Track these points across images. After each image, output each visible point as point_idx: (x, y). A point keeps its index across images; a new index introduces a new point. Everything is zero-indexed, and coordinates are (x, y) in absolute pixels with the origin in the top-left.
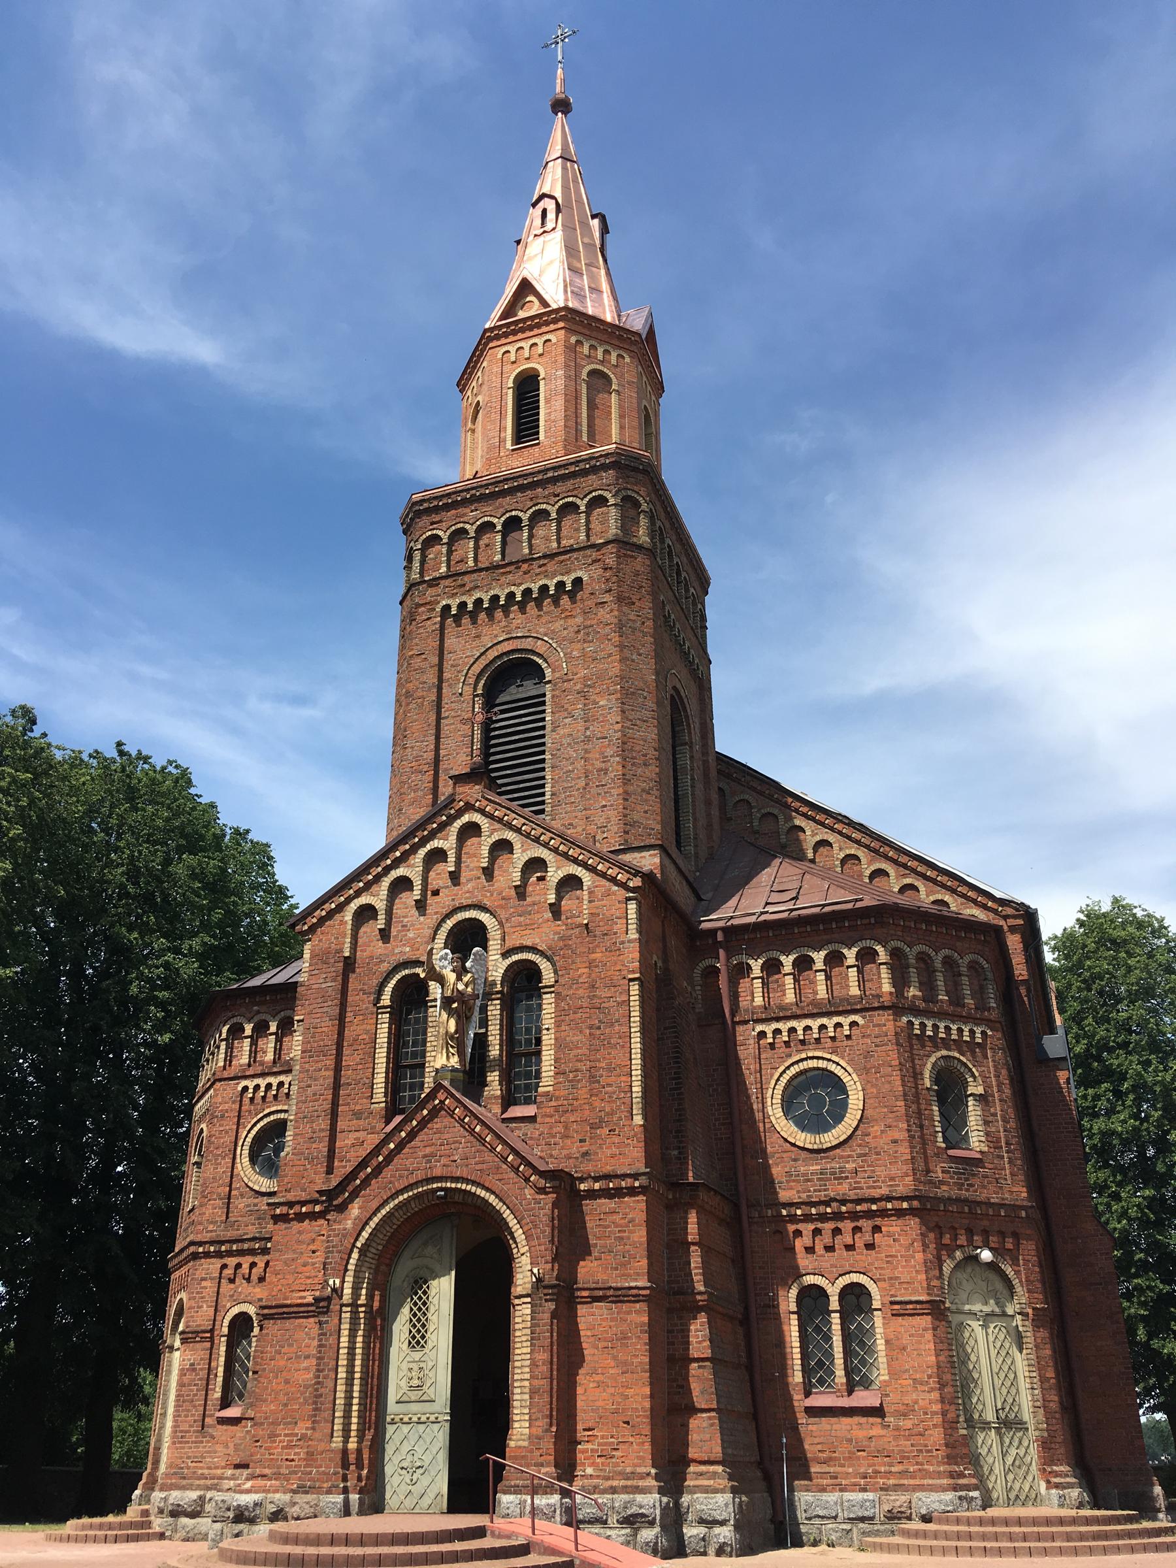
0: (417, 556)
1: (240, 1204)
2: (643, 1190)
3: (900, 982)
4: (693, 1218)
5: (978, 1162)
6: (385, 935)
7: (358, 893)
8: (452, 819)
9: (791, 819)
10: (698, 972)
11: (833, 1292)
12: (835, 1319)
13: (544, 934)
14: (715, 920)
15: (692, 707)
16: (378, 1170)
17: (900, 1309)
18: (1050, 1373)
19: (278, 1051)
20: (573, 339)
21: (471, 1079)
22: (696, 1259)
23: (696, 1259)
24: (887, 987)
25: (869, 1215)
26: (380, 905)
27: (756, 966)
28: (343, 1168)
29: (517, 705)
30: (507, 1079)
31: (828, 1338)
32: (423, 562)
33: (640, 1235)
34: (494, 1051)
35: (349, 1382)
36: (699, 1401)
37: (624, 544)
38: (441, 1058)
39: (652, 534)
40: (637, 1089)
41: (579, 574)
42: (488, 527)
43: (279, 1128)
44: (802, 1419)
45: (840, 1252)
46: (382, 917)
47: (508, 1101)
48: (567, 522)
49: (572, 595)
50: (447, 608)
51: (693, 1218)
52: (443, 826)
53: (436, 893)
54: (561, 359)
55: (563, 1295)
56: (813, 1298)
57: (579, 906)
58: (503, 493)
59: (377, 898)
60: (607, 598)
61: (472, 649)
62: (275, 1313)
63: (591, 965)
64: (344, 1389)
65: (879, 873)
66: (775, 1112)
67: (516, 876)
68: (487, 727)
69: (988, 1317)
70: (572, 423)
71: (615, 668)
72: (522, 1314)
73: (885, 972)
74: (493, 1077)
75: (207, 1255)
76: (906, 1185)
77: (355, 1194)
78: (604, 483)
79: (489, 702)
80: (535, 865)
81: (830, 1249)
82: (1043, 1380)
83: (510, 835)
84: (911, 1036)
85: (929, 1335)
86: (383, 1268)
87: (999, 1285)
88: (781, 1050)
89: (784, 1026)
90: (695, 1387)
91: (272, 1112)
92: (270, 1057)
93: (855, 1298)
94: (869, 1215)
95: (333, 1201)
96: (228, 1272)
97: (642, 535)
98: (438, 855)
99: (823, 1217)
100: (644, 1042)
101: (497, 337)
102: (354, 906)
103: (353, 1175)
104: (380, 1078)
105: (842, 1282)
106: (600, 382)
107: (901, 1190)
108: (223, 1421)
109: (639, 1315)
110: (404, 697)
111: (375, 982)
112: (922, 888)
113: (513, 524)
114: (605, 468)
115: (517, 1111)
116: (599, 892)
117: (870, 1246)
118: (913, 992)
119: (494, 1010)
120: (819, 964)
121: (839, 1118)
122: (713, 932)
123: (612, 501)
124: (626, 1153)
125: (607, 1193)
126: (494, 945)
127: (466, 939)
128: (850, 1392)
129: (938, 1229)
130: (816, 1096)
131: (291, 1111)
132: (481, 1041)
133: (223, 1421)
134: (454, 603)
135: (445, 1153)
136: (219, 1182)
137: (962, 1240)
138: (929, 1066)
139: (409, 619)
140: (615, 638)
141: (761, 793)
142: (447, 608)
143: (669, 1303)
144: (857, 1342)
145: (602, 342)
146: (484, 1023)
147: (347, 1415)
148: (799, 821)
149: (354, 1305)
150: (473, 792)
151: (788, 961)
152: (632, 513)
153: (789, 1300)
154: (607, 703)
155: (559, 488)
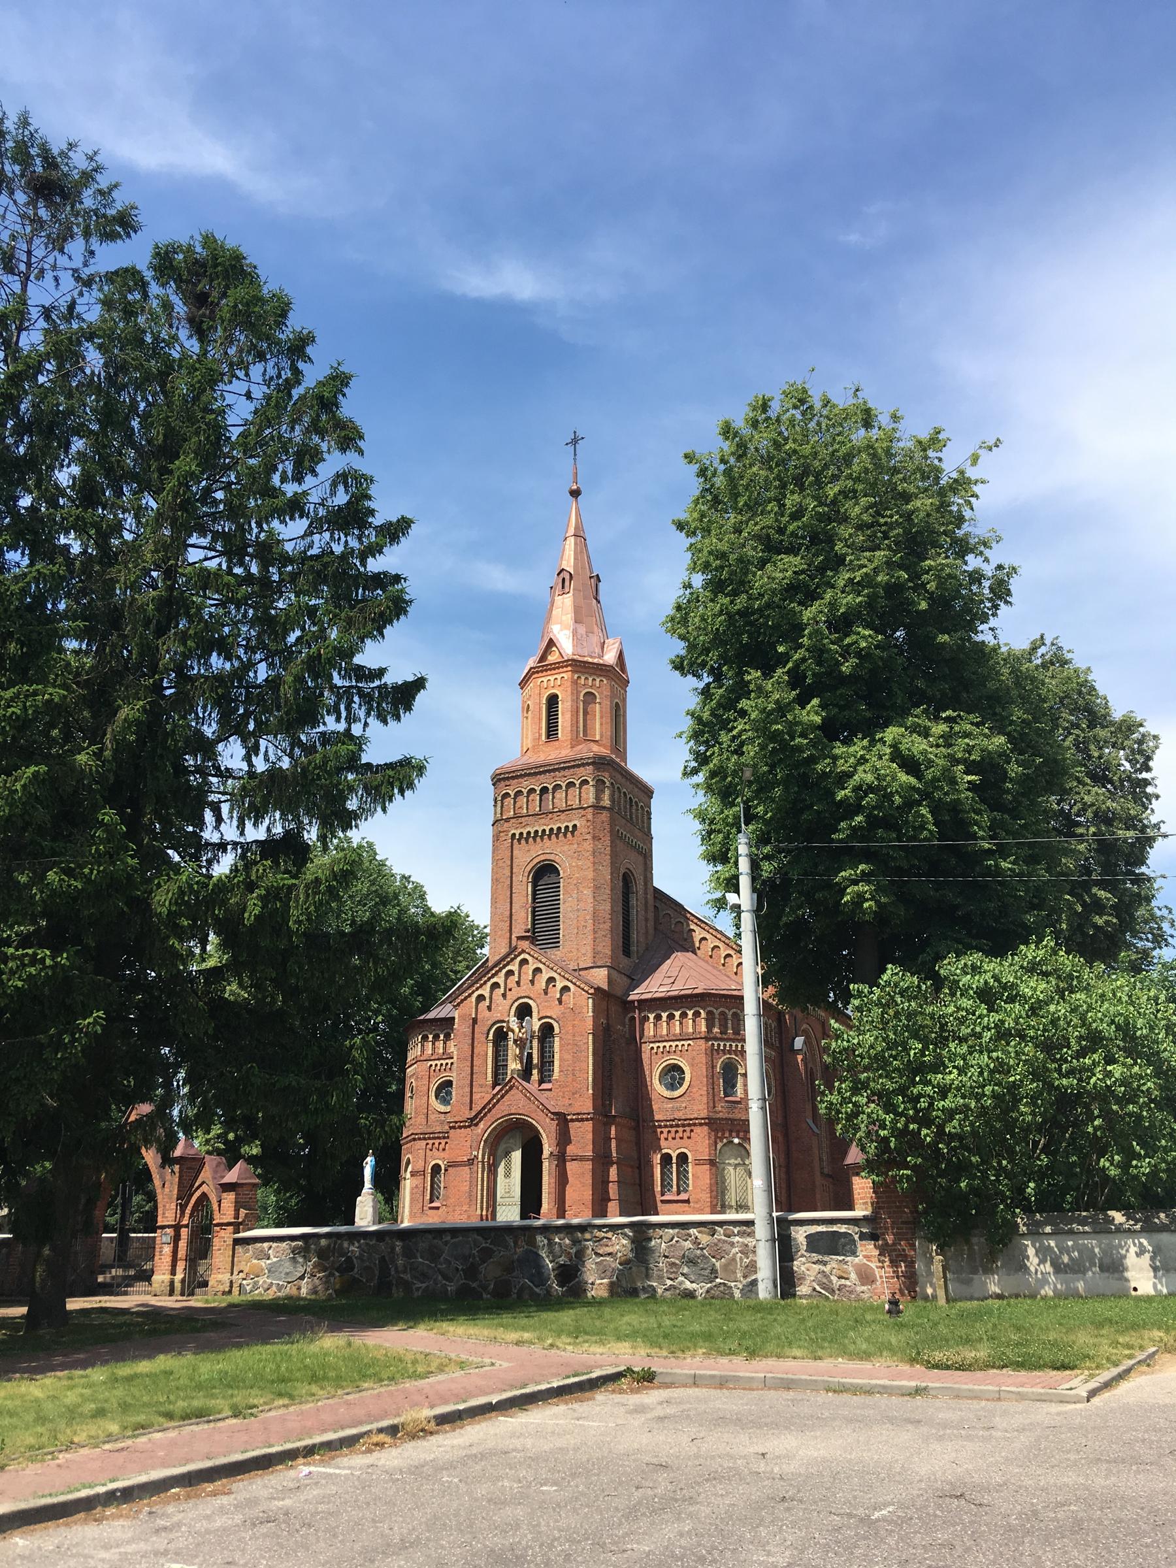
0: (499, 803)
1: (432, 1117)
2: (592, 1119)
3: (710, 1027)
4: (613, 1128)
6: (489, 1008)
7: (477, 989)
8: (516, 956)
9: (688, 925)
10: (627, 1020)
11: (674, 1156)
12: (674, 1166)
13: (555, 1011)
14: (634, 996)
16: (490, 1110)
17: (698, 1163)
19: (445, 1048)
20: (576, 676)
21: (526, 1074)
22: (613, 1144)
23: (613, 1144)
24: (704, 1029)
25: (689, 1125)
26: (487, 995)
27: (651, 1016)
28: (477, 1108)
30: (541, 1072)
32: (502, 807)
33: (590, 1136)
34: (535, 1061)
35: (482, 1190)
36: (612, 1196)
37: (597, 807)
38: (514, 1066)
39: (612, 799)
40: (590, 1079)
41: (575, 822)
42: (532, 791)
43: (449, 1084)
44: (659, 1204)
45: (678, 1139)
46: (488, 1000)
47: (541, 1082)
48: (571, 791)
49: (572, 833)
50: (514, 835)
51: (613, 1128)
52: (512, 960)
54: (569, 689)
55: (561, 1159)
56: (666, 1159)
57: (568, 998)
58: (540, 773)
59: (485, 991)
60: (588, 837)
61: (528, 857)
62: (452, 1165)
63: (573, 1026)
64: (480, 1192)
65: (729, 956)
66: (656, 1082)
67: (544, 984)
69: (736, 1166)
71: (590, 874)
72: (546, 1164)
73: (703, 1023)
74: (535, 1072)
75: (420, 1139)
76: (704, 1114)
77: (481, 1119)
78: (587, 772)
79: (535, 885)
80: (551, 980)
81: (674, 1139)
83: (541, 966)
84: (712, 1050)
87: (743, 1152)
88: (660, 1055)
89: (661, 1045)
90: (611, 1191)
91: (444, 1076)
92: (441, 1051)
93: (683, 1158)
94: (689, 1125)
95: (473, 1122)
96: (430, 1146)
97: (606, 802)
98: (510, 973)
99: (672, 1126)
100: (594, 1060)
101: (538, 672)
102: (476, 994)
103: (480, 1112)
104: (489, 1071)
105: (678, 1151)
106: (590, 698)
107: (702, 1116)
108: (431, 1208)
109: (588, 1166)
110: (495, 881)
111: (486, 1029)
113: (544, 790)
114: (588, 764)
115: (544, 1086)
117: (689, 1138)
118: (716, 1030)
119: (535, 1043)
120: (677, 1017)
121: (681, 1085)
122: (633, 1002)
124: (585, 1105)
125: (577, 1120)
126: (535, 1014)
127: (524, 1012)
128: (678, 1194)
129: (716, 1131)
130: (673, 1075)
131: (453, 1076)
132: (530, 1055)
133: (431, 1208)
134: (517, 832)
135: (515, 1104)
136: (420, 1107)
137: (727, 1135)
139: (496, 838)
140: (591, 858)
142: (514, 835)
143: (601, 1160)
144: (682, 1175)
145: (591, 674)
146: (531, 1048)
147: (482, 1202)
148: (692, 927)
149: (483, 1162)
150: (525, 944)
151: (664, 1015)
152: (601, 787)
153: (657, 1159)
154: (588, 892)
155: (566, 773)
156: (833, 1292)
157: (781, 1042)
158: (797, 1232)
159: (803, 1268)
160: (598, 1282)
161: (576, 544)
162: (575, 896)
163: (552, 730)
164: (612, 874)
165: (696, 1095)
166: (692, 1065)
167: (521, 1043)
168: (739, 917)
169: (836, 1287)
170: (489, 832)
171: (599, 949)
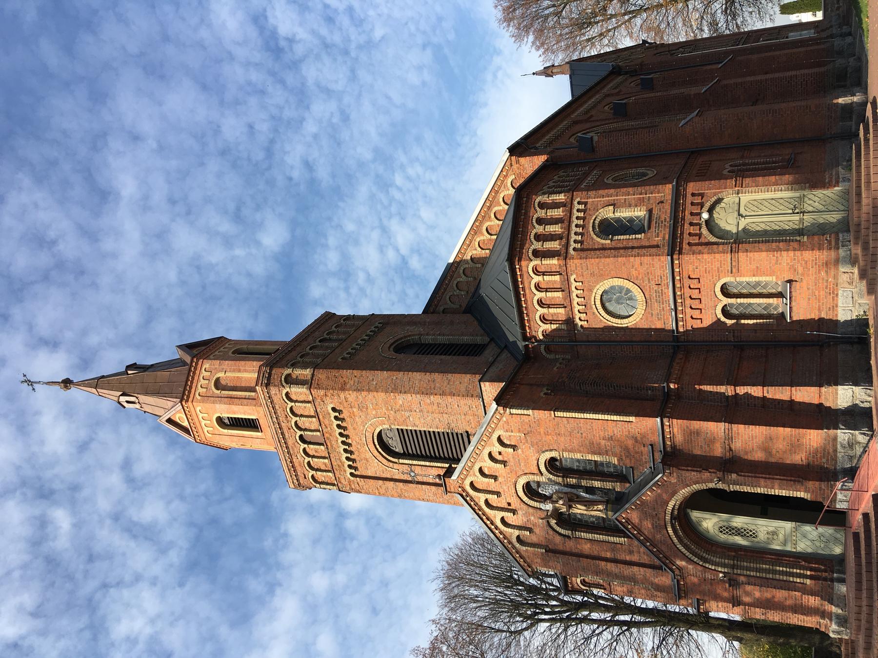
5: (650, 211)
10: (551, 356)
15: (400, 333)
18: (773, 179)
24: (554, 261)
29: (403, 442)
31: (750, 304)
39: (305, 368)
49: (340, 412)
53: (509, 504)
61: (374, 463)
70: (245, 401)
71: (381, 396)
82: (776, 184)
84: (582, 250)
85: (750, 255)
86: (714, 548)
97: (307, 373)
112: (496, 208)
116: (506, 427)
123: (288, 389)
134: (349, 471)
138: (599, 240)
141: (445, 290)
142: (352, 474)
154: (401, 399)
162: (407, 414)
164: (382, 369)
165: (642, 270)
166: (602, 277)
167: (572, 500)
171: (463, 389)
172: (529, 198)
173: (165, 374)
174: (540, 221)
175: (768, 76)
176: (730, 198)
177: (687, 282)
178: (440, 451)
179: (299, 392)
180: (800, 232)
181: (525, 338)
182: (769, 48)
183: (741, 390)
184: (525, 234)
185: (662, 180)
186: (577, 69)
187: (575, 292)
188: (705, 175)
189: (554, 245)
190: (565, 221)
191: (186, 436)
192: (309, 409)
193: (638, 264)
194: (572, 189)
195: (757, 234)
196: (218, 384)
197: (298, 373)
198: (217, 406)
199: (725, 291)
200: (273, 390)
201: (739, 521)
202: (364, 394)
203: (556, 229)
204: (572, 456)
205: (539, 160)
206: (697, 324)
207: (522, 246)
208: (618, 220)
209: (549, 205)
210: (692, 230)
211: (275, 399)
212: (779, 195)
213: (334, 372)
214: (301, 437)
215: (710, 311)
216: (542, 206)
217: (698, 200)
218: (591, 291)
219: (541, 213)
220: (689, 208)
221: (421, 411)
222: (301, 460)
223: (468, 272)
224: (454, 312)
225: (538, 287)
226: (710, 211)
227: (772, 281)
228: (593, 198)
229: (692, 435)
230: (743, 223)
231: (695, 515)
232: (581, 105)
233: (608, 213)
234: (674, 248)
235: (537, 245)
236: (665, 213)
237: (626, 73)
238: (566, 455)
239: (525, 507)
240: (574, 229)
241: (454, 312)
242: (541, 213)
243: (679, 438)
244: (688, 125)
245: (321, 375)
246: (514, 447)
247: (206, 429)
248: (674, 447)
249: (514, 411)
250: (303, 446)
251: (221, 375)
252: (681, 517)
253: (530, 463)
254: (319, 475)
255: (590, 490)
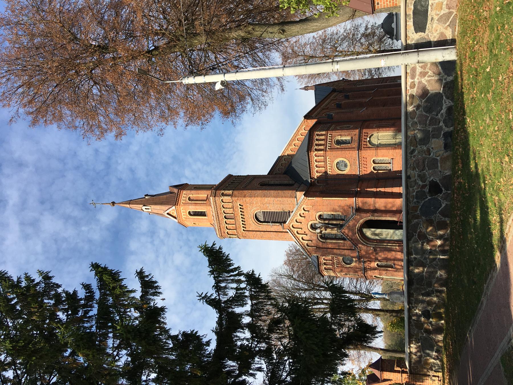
5: (352, 137)
15: (261, 180)
18: (388, 129)
24: (322, 152)
29: (264, 217)
49: (242, 206)
61: (252, 225)
63: (320, 205)
68: (272, 222)
71: (259, 199)
72: (376, 218)
97: (230, 192)
110: (262, 238)
139: (245, 237)
142: (243, 230)
154: (266, 199)
156: (450, 13)
157: (329, 123)
158: (413, 39)
159: (435, 34)
160: (439, 169)
161: (133, 204)
162: (268, 205)
163: (203, 214)
164: (259, 190)
165: (350, 155)
168: (311, 176)
169: (447, 11)
170: (242, 240)
171: (289, 195)
172: (313, 133)
173: (165, 196)
174: (317, 140)
175: (389, 97)
176: (375, 134)
177: (363, 159)
178: (279, 218)
179: (226, 199)
180: (395, 144)
181: (311, 178)
182: (390, 86)
183: (378, 190)
184: (312, 144)
185: (356, 128)
186: (318, 89)
187: (328, 162)
188: (368, 127)
189: (322, 147)
190: (325, 140)
191: (175, 219)
192: (230, 205)
193: (347, 153)
194: (327, 130)
195: (383, 145)
196: (189, 199)
197: (227, 192)
198: (190, 207)
199: (374, 162)
200: (217, 198)
201: (378, 231)
202: (253, 198)
203: (322, 142)
204: (326, 213)
205: (314, 121)
206: (366, 173)
207: (311, 148)
208: (342, 140)
209: (320, 135)
210: (365, 143)
211: (217, 202)
212: (390, 134)
213: (241, 191)
214: (225, 217)
215: (369, 169)
216: (317, 135)
217: (366, 134)
218: (333, 162)
219: (317, 137)
220: (364, 137)
221: (273, 204)
222: (224, 225)
223: (286, 160)
224: (279, 174)
225: (316, 161)
226: (370, 138)
227: (387, 159)
228: (334, 133)
229: (364, 203)
230: (379, 142)
231: (365, 230)
232: (324, 103)
233: (339, 138)
234: (359, 148)
235: (316, 147)
236: (356, 138)
237: (338, 91)
238: (325, 213)
239: (310, 233)
240: (328, 142)
241: (279, 174)
242: (317, 137)
243: (360, 205)
244: (363, 112)
245: (236, 192)
246: (308, 211)
247: (183, 216)
248: (359, 207)
249: (309, 198)
250: (225, 220)
251: (190, 196)
252: (360, 231)
253: (313, 219)
254: (230, 232)
255: (332, 224)
